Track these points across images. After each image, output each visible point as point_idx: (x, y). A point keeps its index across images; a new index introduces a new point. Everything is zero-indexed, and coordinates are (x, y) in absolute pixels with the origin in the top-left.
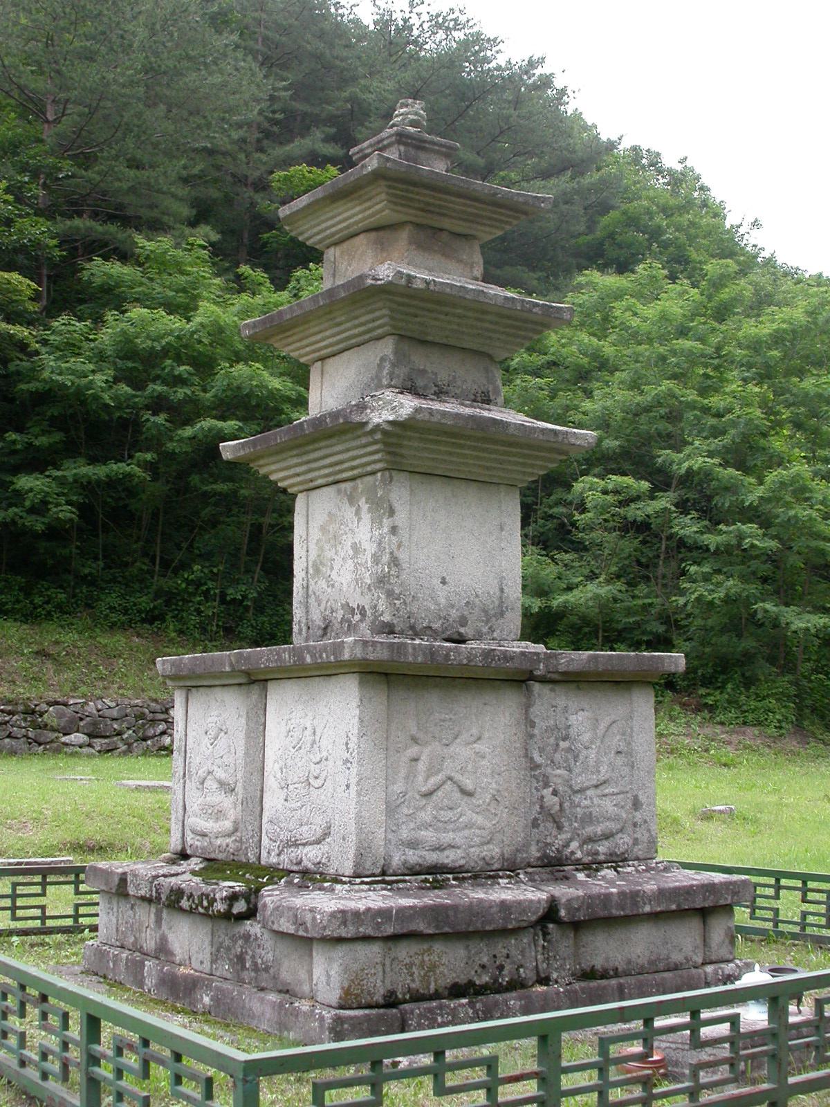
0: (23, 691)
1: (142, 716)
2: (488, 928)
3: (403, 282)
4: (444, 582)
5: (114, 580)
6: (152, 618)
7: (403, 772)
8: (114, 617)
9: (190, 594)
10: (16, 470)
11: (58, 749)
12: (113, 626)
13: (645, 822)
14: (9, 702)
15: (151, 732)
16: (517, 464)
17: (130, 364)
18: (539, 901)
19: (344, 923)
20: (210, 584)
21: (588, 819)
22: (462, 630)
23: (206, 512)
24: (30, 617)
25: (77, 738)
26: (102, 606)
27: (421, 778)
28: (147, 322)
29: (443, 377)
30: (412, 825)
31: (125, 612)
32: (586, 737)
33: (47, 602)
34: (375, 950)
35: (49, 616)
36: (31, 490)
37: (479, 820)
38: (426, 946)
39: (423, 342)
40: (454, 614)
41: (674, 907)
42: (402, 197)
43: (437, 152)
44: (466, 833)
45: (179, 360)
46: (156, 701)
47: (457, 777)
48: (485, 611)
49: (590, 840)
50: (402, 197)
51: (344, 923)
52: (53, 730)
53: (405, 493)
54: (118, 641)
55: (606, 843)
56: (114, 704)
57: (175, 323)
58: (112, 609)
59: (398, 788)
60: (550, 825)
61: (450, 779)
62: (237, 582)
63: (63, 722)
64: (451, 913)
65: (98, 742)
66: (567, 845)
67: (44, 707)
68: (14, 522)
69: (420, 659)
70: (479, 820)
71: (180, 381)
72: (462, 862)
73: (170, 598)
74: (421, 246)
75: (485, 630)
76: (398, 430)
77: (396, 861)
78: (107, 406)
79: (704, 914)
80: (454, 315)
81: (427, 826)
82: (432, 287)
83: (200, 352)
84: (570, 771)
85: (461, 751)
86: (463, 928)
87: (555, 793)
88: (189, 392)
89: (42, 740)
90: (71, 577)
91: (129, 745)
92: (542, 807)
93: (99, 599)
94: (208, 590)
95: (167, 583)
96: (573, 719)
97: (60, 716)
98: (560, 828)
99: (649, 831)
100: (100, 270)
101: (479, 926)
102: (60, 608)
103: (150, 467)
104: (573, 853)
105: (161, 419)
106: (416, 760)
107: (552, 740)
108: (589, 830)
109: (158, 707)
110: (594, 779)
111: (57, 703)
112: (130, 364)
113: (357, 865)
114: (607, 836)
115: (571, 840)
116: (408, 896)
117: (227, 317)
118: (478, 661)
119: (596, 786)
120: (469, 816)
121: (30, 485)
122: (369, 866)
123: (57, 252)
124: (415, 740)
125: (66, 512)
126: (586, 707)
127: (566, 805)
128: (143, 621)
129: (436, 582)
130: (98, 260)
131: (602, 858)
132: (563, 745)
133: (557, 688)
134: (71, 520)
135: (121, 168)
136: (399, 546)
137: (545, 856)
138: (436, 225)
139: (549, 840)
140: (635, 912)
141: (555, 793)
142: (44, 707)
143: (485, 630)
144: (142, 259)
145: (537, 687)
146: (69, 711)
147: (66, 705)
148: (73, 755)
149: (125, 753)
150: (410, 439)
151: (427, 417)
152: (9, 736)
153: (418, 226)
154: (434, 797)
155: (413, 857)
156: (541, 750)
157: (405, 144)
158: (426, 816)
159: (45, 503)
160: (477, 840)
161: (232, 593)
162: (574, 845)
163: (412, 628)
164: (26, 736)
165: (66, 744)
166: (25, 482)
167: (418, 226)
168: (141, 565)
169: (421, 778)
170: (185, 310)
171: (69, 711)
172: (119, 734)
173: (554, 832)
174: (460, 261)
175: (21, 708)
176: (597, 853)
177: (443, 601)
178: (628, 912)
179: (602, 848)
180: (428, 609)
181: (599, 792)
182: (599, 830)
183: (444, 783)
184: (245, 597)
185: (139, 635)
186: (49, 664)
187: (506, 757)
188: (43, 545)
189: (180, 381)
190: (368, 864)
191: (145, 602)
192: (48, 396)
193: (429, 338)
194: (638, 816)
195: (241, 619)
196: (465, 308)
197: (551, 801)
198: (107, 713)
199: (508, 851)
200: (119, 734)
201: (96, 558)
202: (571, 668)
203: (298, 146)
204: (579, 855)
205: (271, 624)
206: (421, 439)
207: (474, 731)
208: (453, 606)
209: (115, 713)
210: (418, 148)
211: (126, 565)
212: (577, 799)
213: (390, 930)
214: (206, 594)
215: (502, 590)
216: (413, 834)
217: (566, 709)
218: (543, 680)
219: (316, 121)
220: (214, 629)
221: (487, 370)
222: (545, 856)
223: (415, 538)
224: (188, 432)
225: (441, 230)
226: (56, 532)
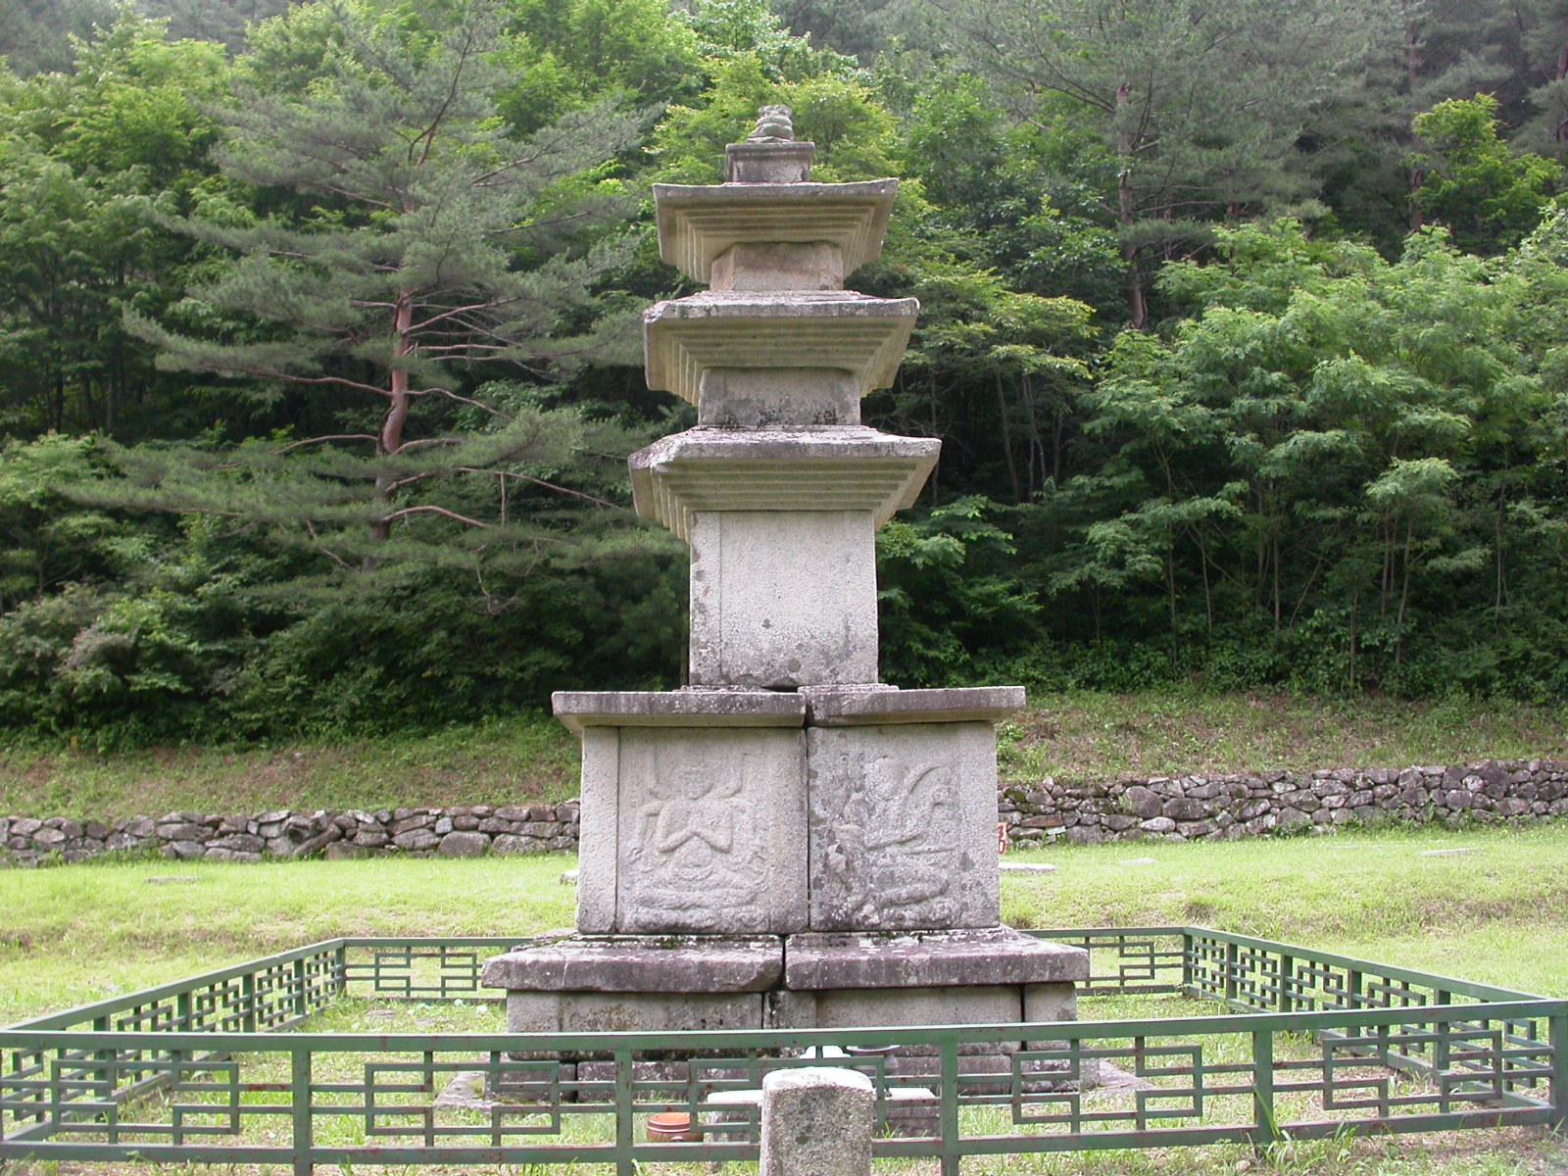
0: (1098, 772)
1: (1240, 794)
2: (683, 989)
3: (676, 314)
4: (767, 625)
5: (1227, 636)
6: (1275, 676)
7: (638, 827)
8: (1225, 679)
9: (1317, 644)
10: (1091, 519)
11: (1139, 836)
12: (1225, 690)
13: (979, 884)
14: (1078, 785)
15: (1250, 812)
16: (849, 486)
17: (1211, 377)
18: (752, 965)
19: (508, 974)
20: (1340, 630)
21: (889, 879)
22: (793, 676)
23: (1327, 542)
24: (1125, 686)
25: (1161, 822)
26: (1212, 667)
27: (659, 834)
28: (1228, 324)
29: (772, 402)
30: (646, 883)
31: (1241, 671)
32: (886, 787)
33: (1148, 667)
34: (550, 1004)
35: (1148, 683)
36: (1103, 539)
37: (737, 878)
38: (614, 1004)
39: (745, 370)
40: (781, 658)
41: (955, 981)
42: (711, 221)
43: (788, 158)
44: (718, 892)
45: (1272, 367)
46: (1258, 775)
47: (707, 833)
48: (825, 653)
49: (891, 903)
50: (711, 221)
51: (508, 974)
52: (1131, 814)
53: (714, 535)
54: (1227, 707)
55: (917, 908)
56: (1202, 782)
57: (1265, 323)
58: (1222, 669)
59: (634, 843)
60: (836, 886)
61: (697, 834)
62: (1376, 624)
63: (1142, 805)
64: (636, 971)
65: (1185, 827)
66: (859, 907)
67: (1119, 788)
68: (1092, 579)
69: (635, 710)
70: (737, 878)
71: (1267, 391)
72: (709, 923)
73: (1293, 652)
74: (750, 266)
75: (825, 673)
76: (676, 472)
77: (628, 920)
78: (1177, 433)
79: (1022, 991)
80: (765, 336)
81: (666, 884)
82: (714, 313)
83: (1296, 353)
84: (862, 825)
85: (713, 805)
86: (651, 987)
87: (840, 850)
88: (1282, 403)
89: (1117, 826)
90: (1170, 637)
91: (1224, 829)
92: (825, 866)
93: (1208, 659)
94: (1338, 637)
95: (1287, 634)
96: (868, 767)
97: (1137, 798)
98: (849, 889)
99: (985, 894)
100: (1180, 273)
101: (671, 986)
102: (1161, 673)
103: (1249, 500)
104: (866, 917)
105: (1247, 439)
106: (656, 815)
107: (841, 792)
108: (890, 892)
109: (1259, 782)
110: (897, 835)
111: (1135, 783)
112: (1211, 377)
113: (581, 921)
114: (919, 900)
115: (863, 903)
116: (124, 909)
117: (1327, 308)
118: (713, 708)
119: (902, 843)
120: (722, 873)
121: (1100, 533)
122: (595, 922)
123: (1120, 263)
124: (654, 794)
125: (1144, 562)
126: (891, 752)
127: (857, 864)
128: (1264, 681)
129: (757, 626)
130: (1170, 264)
131: (909, 923)
132: (855, 796)
133: (849, 734)
134: (1155, 571)
135: (1189, 151)
136: (706, 592)
137: (829, 919)
138: (767, 239)
139: (835, 902)
140: (893, 983)
141: (840, 850)
142: (1119, 788)
143: (825, 673)
144: (1226, 254)
145: (818, 734)
146: (1149, 792)
147: (1145, 785)
148: (1154, 842)
149: (1218, 838)
150: (697, 478)
151: (696, 453)
152: (1078, 823)
153: (748, 245)
154: (677, 854)
155: (646, 915)
156: (826, 804)
157: (743, 159)
158: (665, 873)
159: (1121, 552)
160: (733, 901)
161: (1368, 639)
162: (868, 909)
163: (725, 677)
164: (1098, 822)
165: (1145, 830)
166: (1099, 531)
167: (748, 245)
168: (1258, 615)
169: (659, 834)
170: (1278, 306)
171: (1149, 792)
172: (1212, 815)
173: (843, 894)
174: (802, 272)
175: (1091, 791)
176: (902, 918)
177: (766, 646)
178: (883, 983)
179: (910, 914)
180: (747, 656)
181: (906, 849)
182: (904, 892)
183: (688, 839)
184: (1384, 643)
185: (1258, 698)
186: (1133, 740)
187: (772, 811)
188: (1132, 602)
189: (1267, 391)
190: (595, 921)
191: (1263, 658)
192: (1127, 428)
193: (748, 365)
194: (967, 877)
195: (1386, 669)
196: (773, 326)
197: (837, 859)
198: (1195, 792)
199: (774, 913)
200: (1212, 815)
201: (1204, 611)
202: (853, 711)
203: (1449, 77)
204: (875, 919)
205: (1425, 673)
206: (713, 477)
207: (733, 784)
208: (779, 650)
209: (1205, 791)
210: (760, 159)
211: (1240, 616)
212: (871, 857)
213: (560, 984)
214: (1336, 643)
215: (848, 628)
216: (648, 892)
217: (861, 756)
218: (826, 726)
219: (1464, 40)
220: (1351, 683)
221: (832, 387)
222: (829, 919)
223: (726, 582)
224: (1280, 451)
225: (778, 243)
226: (1143, 586)
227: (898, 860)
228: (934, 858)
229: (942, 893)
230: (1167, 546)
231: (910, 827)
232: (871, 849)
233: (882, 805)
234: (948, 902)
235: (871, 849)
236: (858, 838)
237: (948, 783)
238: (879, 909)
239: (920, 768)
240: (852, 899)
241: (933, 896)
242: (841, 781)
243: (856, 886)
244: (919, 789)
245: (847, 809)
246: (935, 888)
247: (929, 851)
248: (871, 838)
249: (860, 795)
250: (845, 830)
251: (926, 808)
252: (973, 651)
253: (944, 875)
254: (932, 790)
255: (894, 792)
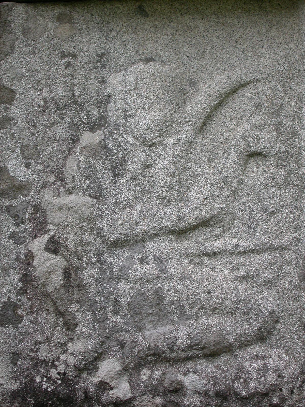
21: (154, 306)
32: (147, 119)
49: (156, 357)
55: (209, 367)
60: (46, 319)
66: (90, 364)
84: (100, 197)
92: (26, 278)
96: (116, 82)
98: (70, 326)
104: (104, 386)
107: (61, 130)
108: (154, 335)
110: (170, 216)
127: (88, 274)
132: (88, 139)
141: (53, 247)
156: (29, 154)
162: (108, 368)
173: (59, 336)
181: (189, 244)
182: (182, 334)
212: (118, 260)
227: (177, 269)
228: (247, 265)
229: (262, 337)
230: (56, 238)
231: (198, 200)
232: (116, 245)
233: (140, 155)
234: (276, 358)
235: (116, 245)
236: (91, 222)
237: (276, 112)
238: (131, 370)
239: (220, 82)
240: (77, 346)
241: (245, 344)
242: (61, 108)
243: (84, 320)
244: (218, 125)
245: (71, 163)
246: (248, 328)
247: (236, 252)
248: (117, 224)
249: (97, 137)
250: (66, 207)
251: (230, 161)
252: (94, 357)
253: (268, 301)
254: (243, 125)
255: (165, 129)
